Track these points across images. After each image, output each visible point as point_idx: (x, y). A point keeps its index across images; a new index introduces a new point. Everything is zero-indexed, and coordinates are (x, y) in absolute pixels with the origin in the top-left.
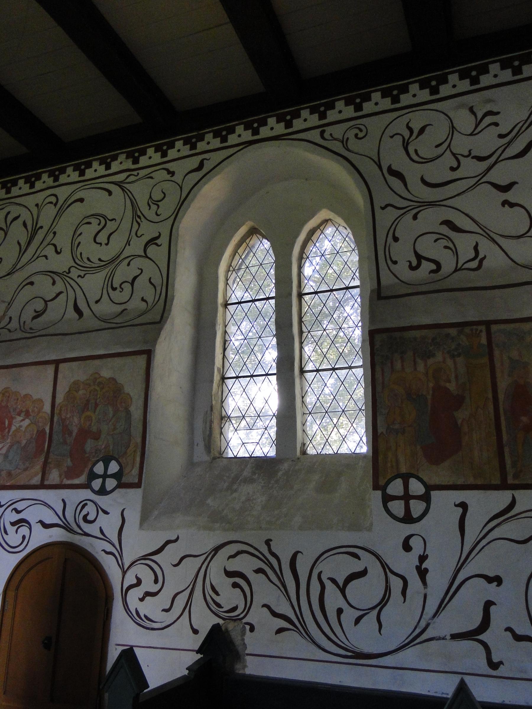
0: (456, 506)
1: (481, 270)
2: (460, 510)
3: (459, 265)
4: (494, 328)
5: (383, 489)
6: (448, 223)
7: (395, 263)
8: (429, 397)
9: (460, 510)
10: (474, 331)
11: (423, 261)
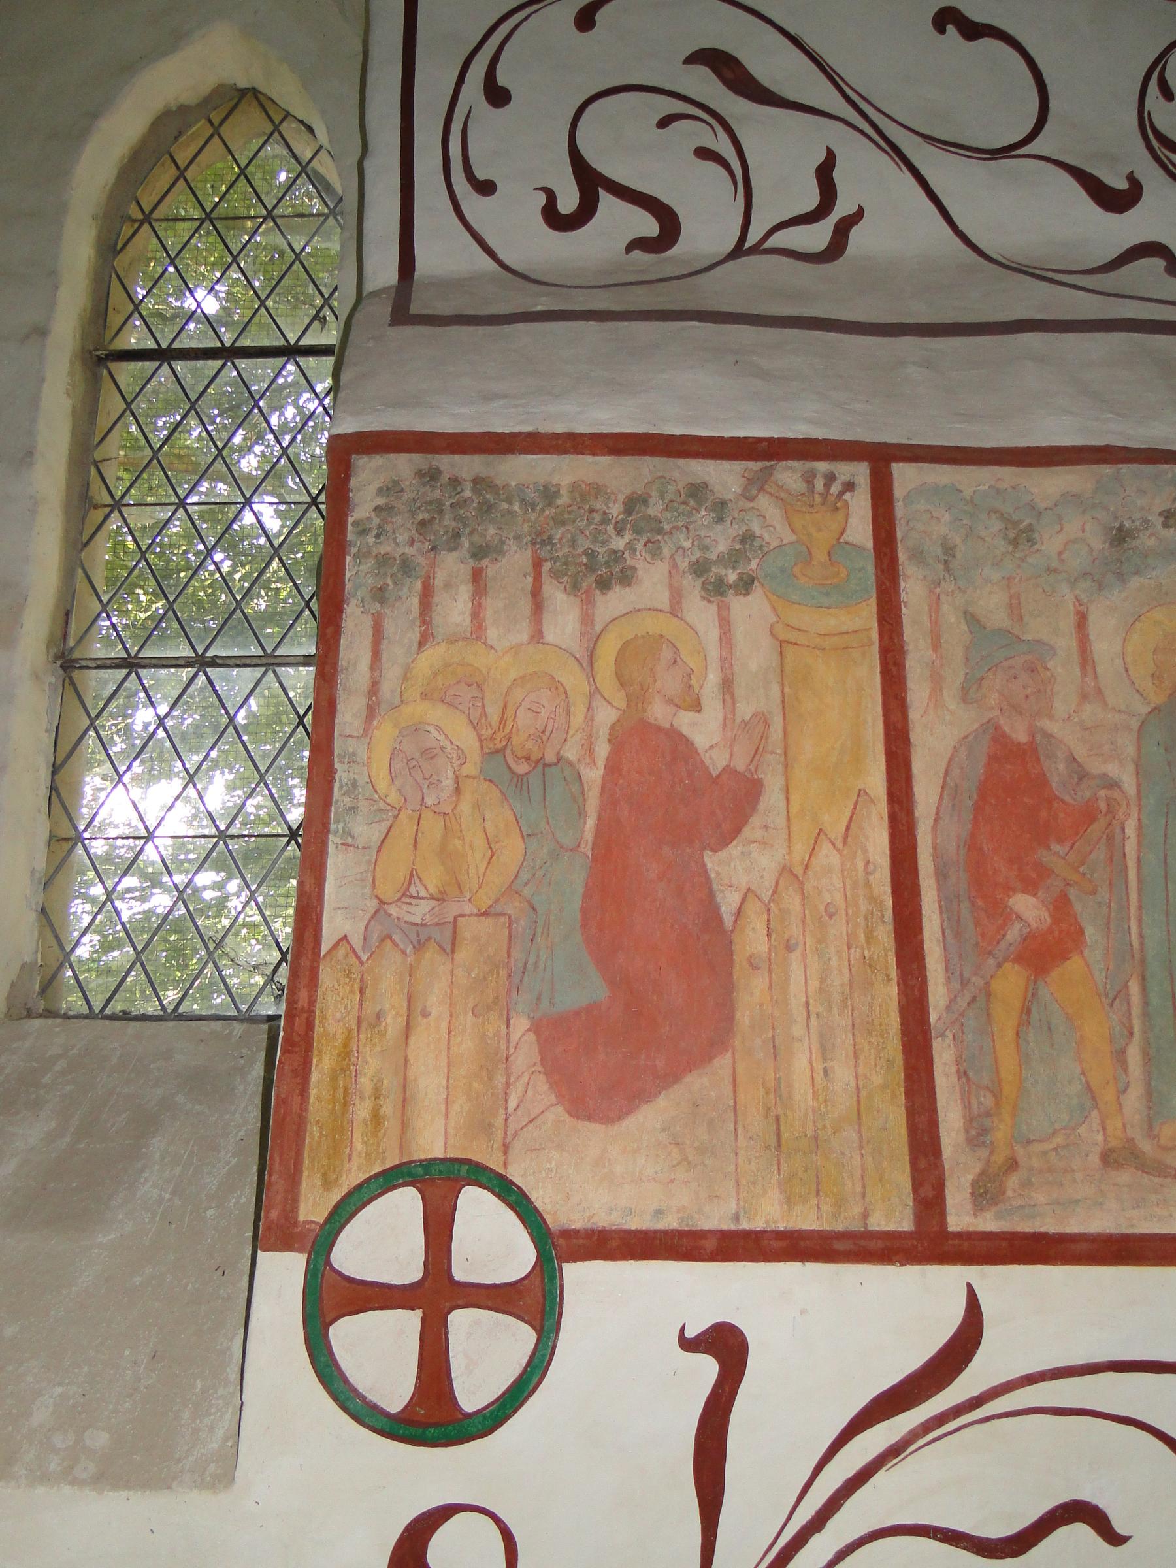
0: (688, 1345)
2: (707, 1368)
3: (752, 239)
5: (319, 1244)
6: (720, 63)
7: (486, 188)
8: (594, 775)
9: (707, 1368)
10: (819, 484)
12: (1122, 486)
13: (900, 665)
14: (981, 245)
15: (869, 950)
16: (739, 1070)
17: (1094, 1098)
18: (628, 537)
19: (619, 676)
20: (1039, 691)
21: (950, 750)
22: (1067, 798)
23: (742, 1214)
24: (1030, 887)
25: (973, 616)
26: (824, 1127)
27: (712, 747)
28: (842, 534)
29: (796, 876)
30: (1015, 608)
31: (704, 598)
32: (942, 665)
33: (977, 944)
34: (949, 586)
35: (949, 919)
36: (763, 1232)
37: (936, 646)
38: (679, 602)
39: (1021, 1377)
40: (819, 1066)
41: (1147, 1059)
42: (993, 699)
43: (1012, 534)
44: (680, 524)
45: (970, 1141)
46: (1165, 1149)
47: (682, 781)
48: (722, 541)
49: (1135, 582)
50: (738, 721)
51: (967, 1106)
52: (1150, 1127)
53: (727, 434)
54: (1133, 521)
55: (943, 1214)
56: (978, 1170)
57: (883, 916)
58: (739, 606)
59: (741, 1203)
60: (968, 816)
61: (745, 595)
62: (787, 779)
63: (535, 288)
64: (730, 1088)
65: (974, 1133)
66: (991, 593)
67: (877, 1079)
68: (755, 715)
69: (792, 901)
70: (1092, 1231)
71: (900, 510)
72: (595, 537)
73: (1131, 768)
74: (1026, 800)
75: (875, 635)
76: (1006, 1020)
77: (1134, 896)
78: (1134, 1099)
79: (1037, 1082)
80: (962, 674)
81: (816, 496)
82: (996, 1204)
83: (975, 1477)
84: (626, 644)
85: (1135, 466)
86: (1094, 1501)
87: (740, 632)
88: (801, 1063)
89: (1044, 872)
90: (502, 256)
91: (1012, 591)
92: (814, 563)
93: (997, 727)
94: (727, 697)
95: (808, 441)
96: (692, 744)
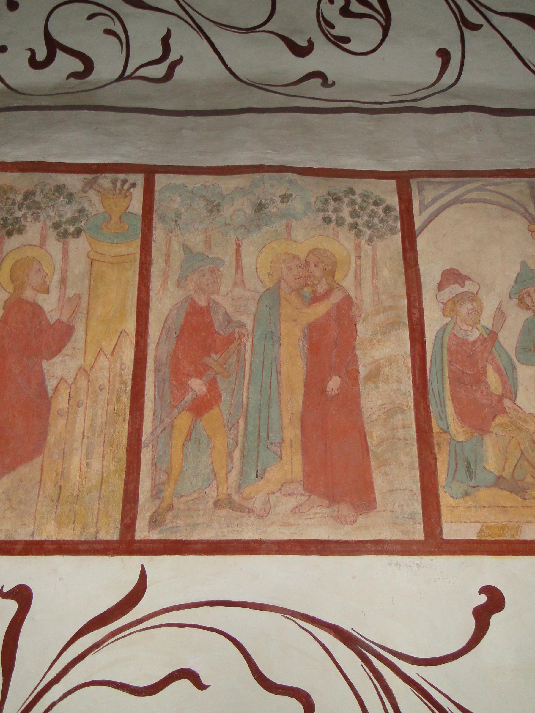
1: (170, 82)
3: (129, 72)
4: (161, 180)
10: (119, 185)
11: (60, 54)
12: (264, 184)
13: (148, 270)
14: (238, 74)
15: (117, 406)
16: (45, 464)
17: (215, 475)
18: (24, 211)
19: (11, 277)
20: (214, 281)
21: (169, 310)
22: (221, 333)
23: (35, 532)
24: (199, 375)
25: (187, 246)
26: (83, 491)
27: (51, 311)
28: (128, 208)
29: (86, 372)
30: (208, 243)
31: (56, 240)
32: (169, 270)
33: (170, 402)
34: (177, 232)
35: (158, 391)
36: (45, 541)
37: (167, 261)
38: (45, 242)
39: (163, 609)
40: (84, 462)
41: (243, 456)
42: (191, 286)
43: (210, 208)
44: (50, 204)
45: (152, 496)
46: (246, 499)
47: (36, 327)
48: (69, 212)
49: (265, 229)
50: (66, 298)
51: (154, 480)
52: (239, 489)
53: (78, 162)
54: (266, 200)
55: (134, 531)
56: (153, 510)
57: (126, 390)
58: (73, 243)
59: (36, 528)
60: (173, 342)
61: (77, 238)
62: (87, 326)
63: (16, 95)
64: (39, 473)
65: (155, 492)
66: (197, 235)
67: (112, 468)
68: (75, 295)
69: (83, 383)
70: (204, 538)
71: (157, 196)
72: (8, 211)
73: (252, 317)
74: (202, 334)
75: (138, 256)
76: (178, 438)
77: (247, 378)
78: (234, 475)
79: (189, 467)
80: (178, 275)
81: (117, 190)
82: (160, 526)
83: (138, 656)
84: (16, 262)
85: (271, 174)
86: (193, 669)
87: (72, 255)
88: (76, 461)
89: (207, 367)
90: (7, 81)
91: (207, 234)
92: (113, 222)
93: (192, 299)
94: (62, 287)
95: (116, 164)
96: (43, 309)
